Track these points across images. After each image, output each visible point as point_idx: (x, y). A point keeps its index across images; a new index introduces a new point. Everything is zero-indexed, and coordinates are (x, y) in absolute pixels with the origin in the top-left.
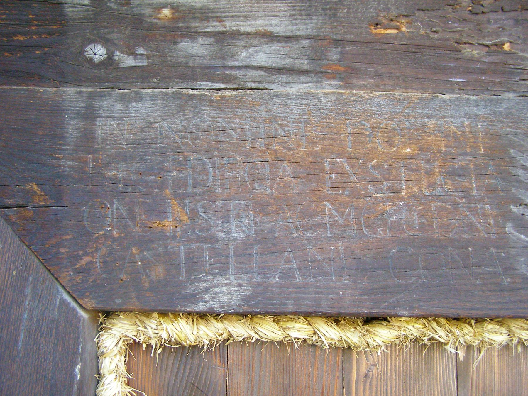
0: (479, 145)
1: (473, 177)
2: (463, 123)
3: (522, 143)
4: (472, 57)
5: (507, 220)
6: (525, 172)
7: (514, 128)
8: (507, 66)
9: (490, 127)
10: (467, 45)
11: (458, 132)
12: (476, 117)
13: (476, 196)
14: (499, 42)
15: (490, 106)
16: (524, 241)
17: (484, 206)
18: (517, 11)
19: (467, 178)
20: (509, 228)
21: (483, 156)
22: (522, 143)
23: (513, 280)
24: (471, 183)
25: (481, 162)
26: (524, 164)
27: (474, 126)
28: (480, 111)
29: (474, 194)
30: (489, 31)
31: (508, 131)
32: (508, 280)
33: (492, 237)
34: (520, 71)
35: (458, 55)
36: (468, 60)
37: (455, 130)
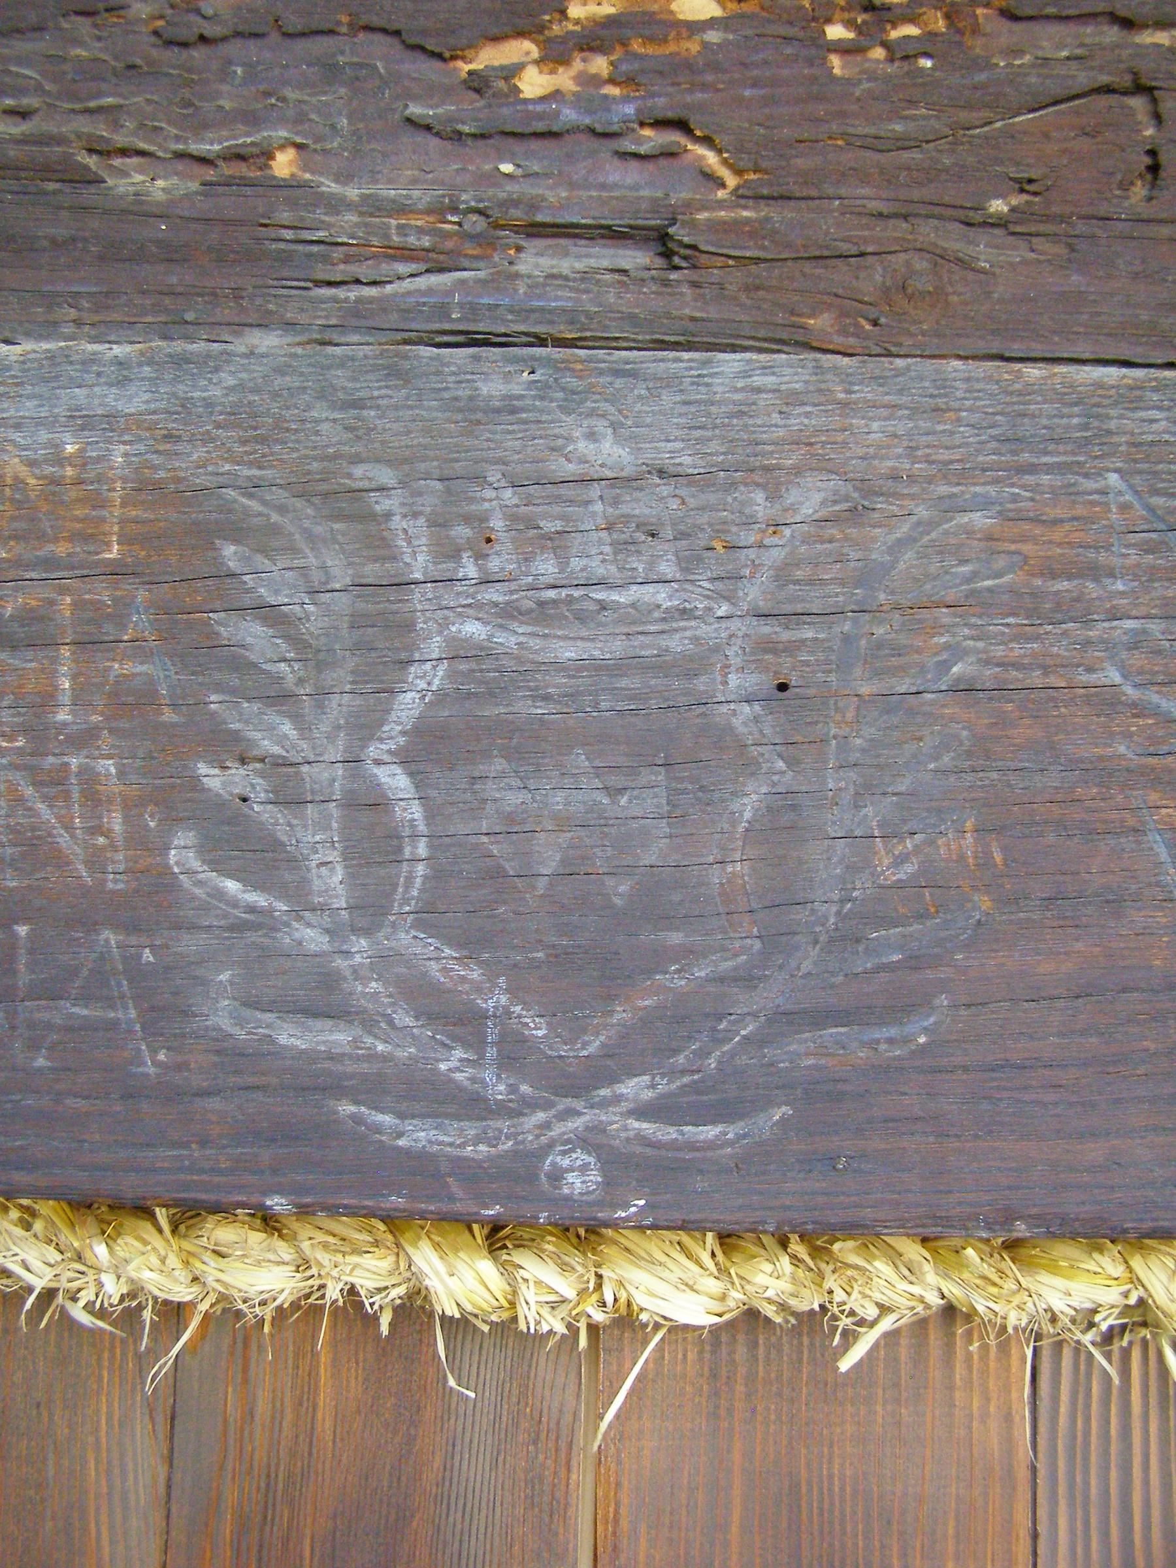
0: (107, 528)
1: (65, 652)
2: (58, 446)
3: (275, 517)
4: (142, 203)
5: (172, 821)
6: (271, 632)
7: (250, 464)
8: (272, 233)
9: (156, 460)
10: (135, 160)
11: (32, 481)
12: (111, 423)
13: (65, 724)
14: (253, 144)
15: (176, 380)
16: (235, 904)
17: (92, 763)
18: (331, 32)
19: (40, 654)
20: (183, 853)
21: (116, 572)
22: (275, 517)
23: (179, 1059)
24: (53, 675)
25: (103, 593)
26: (272, 600)
27: (99, 459)
28: (131, 398)
29: (63, 716)
30: (221, 107)
31: (228, 473)
32: (161, 1057)
33: (110, 885)
34: (315, 249)
35: (89, 195)
36: (124, 212)
37: (23, 471)
